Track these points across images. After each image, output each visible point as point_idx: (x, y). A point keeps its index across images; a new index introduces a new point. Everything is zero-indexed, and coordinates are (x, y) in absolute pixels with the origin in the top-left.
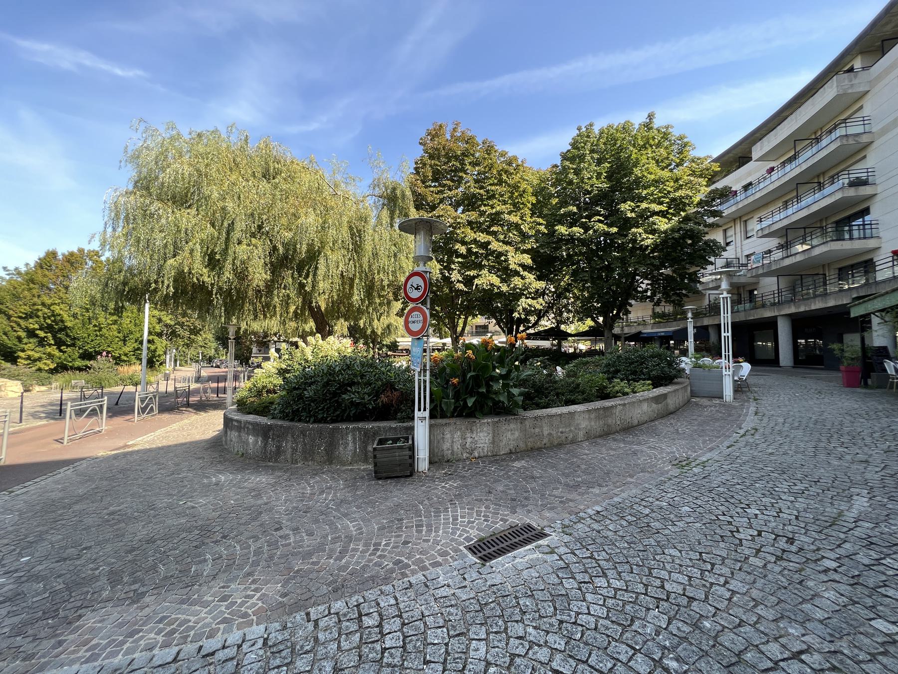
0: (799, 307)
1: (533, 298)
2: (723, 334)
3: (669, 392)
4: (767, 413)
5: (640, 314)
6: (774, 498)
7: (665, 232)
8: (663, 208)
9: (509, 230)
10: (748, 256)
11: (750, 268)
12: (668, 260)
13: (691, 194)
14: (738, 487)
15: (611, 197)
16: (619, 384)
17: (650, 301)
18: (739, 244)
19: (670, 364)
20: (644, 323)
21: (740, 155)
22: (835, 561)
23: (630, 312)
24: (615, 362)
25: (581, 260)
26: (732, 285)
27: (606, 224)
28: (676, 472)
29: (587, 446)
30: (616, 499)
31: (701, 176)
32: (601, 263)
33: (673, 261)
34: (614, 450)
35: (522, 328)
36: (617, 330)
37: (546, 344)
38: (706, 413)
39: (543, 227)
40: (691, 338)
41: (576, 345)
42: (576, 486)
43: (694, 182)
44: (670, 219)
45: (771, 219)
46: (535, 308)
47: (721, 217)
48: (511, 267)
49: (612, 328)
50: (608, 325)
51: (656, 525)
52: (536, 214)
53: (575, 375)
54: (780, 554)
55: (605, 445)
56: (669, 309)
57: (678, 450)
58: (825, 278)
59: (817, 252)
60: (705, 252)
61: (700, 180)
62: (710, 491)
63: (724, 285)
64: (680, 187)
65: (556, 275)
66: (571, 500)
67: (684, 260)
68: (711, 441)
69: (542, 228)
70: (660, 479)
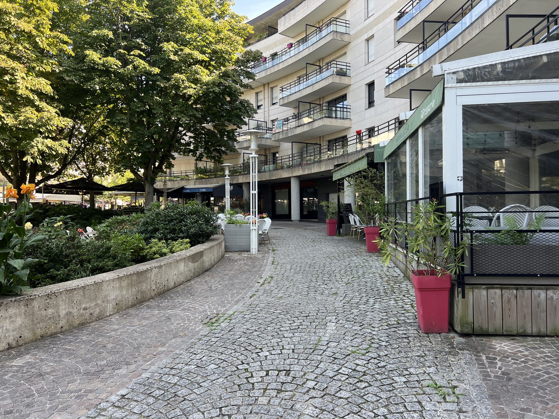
0: (304, 171)
1: (54, 139)
2: (252, 192)
3: (205, 249)
4: (280, 261)
5: (183, 168)
6: (279, 338)
7: (207, 84)
8: (205, 58)
9: (18, 40)
10: (273, 121)
11: (274, 132)
12: (209, 114)
13: (230, 50)
14: (255, 333)
15: (154, 31)
16: (156, 244)
17: (193, 155)
18: (267, 109)
19: (208, 221)
20: (186, 178)
21: (270, 24)
22: (314, 380)
23: (173, 166)
24: (153, 220)
25: (119, 99)
26: (259, 146)
27: (149, 62)
28: (206, 330)
29: (116, 319)
30: (144, 376)
31: (238, 34)
32: (141, 106)
33: (216, 117)
34: (147, 319)
35: (39, 177)
36: (158, 185)
37: (75, 199)
38: (236, 267)
39: (71, 47)
40: (228, 196)
41: (113, 200)
42: (97, 374)
43: (233, 39)
44: (211, 72)
45: (289, 90)
46: (56, 151)
47: (254, 80)
48: (20, 92)
49: (153, 182)
50: (149, 179)
51: (184, 391)
52: (59, 27)
53: (108, 238)
54: (280, 388)
55: (137, 315)
56: (210, 165)
57: (210, 308)
58: (320, 148)
59: (317, 124)
60: (240, 111)
61: (238, 38)
62: (233, 343)
63: (253, 146)
64: (220, 41)
65: (88, 113)
66: (91, 391)
67: (223, 117)
68: (238, 293)
69: (69, 49)
70: (191, 341)
